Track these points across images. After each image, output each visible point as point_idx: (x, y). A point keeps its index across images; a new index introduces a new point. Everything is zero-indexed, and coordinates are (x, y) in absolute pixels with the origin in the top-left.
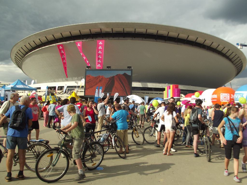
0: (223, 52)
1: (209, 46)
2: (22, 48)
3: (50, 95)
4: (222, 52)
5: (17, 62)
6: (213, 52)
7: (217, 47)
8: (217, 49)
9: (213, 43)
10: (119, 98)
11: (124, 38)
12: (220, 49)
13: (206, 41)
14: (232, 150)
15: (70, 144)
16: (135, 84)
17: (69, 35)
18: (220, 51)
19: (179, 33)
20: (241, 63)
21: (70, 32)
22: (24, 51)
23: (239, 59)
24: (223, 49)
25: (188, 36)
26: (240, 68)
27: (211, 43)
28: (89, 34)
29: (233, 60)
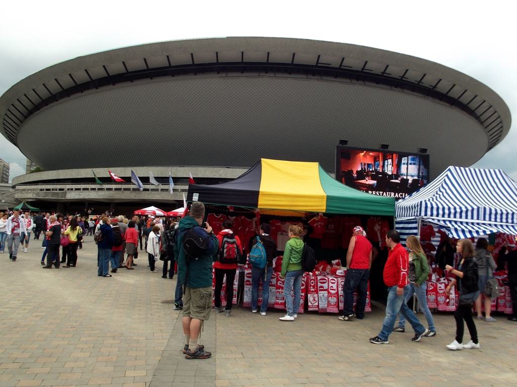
0: (461, 100)
1: (456, 98)
2: (19, 101)
3: (20, 233)
4: (469, 105)
5: (8, 129)
6: (441, 100)
7: (450, 90)
8: (460, 100)
9: (425, 75)
10: (258, 190)
11: (242, 73)
12: (455, 94)
13: (466, 92)
14: (515, 372)
15: (197, 259)
16: (169, 262)
17: (122, 70)
18: (473, 109)
19: (455, 83)
20: (500, 124)
21: (124, 63)
22: (24, 106)
23: (491, 111)
24: (451, 89)
25: (386, 66)
26: (499, 132)
27: (421, 77)
28: (166, 66)
29: (479, 112)
